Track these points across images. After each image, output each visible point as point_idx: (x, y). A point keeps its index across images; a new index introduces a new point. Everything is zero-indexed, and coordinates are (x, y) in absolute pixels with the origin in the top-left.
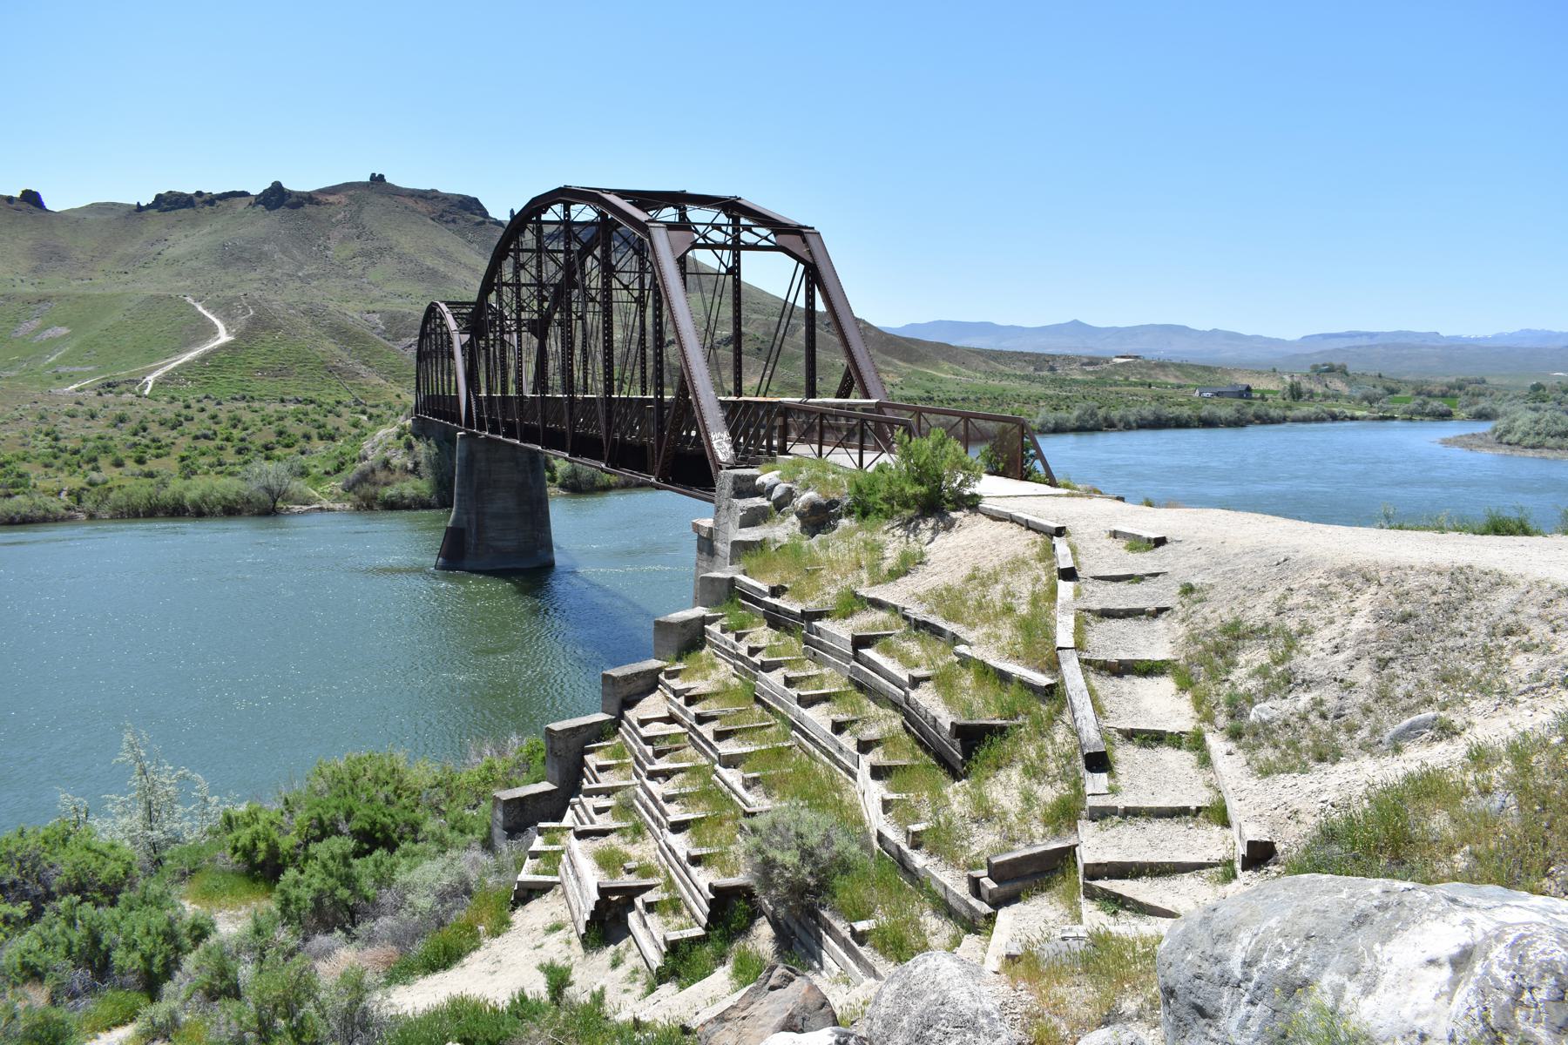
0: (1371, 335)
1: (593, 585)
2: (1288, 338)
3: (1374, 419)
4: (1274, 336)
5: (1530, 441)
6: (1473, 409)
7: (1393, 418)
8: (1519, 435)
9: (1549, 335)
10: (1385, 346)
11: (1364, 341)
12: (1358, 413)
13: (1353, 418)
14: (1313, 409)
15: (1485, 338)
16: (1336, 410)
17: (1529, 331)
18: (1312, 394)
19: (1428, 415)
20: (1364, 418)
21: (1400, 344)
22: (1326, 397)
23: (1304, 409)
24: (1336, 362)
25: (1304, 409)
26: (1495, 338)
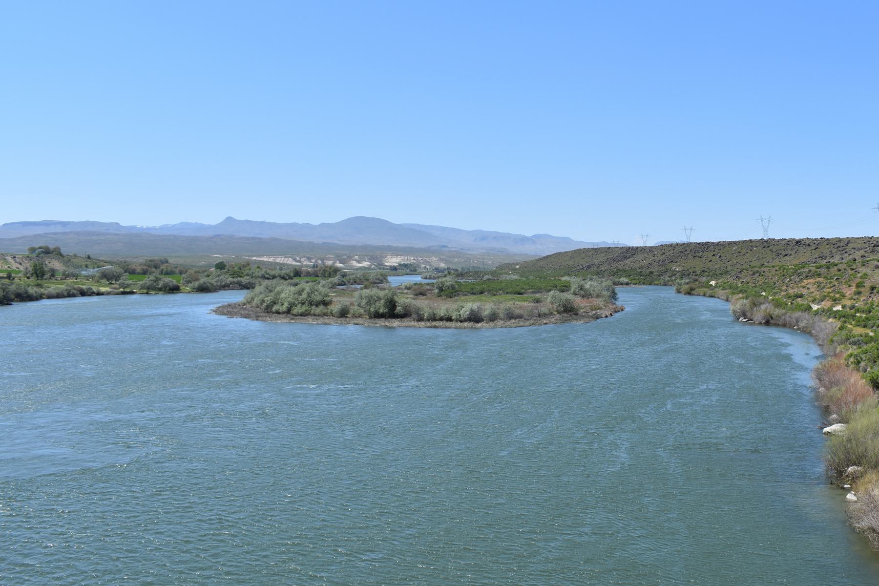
0: (64, 224)
1: (461, 275)
2: (330, 222)
3: (117, 294)
4: (272, 221)
5: (297, 310)
6: (197, 284)
7: (132, 293)
8: (286, 305)
9: (201, 227)
10: (77, 233)
11: (59, 229)
12: (103, 289)
13: (99, 294)
14: (63, 287)
15: (155, 228)
16: (84, 287)
17: (186, 223)
18: (53, 273)
19: (160, 289)
20: (108, 294)
21: (90, 232)
22: (66, 276)
23: (53, 287)
24: (52, 247)
25: (53, 287)
26: (162, 228)
